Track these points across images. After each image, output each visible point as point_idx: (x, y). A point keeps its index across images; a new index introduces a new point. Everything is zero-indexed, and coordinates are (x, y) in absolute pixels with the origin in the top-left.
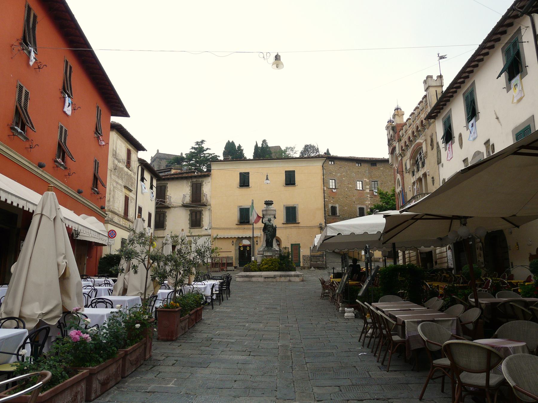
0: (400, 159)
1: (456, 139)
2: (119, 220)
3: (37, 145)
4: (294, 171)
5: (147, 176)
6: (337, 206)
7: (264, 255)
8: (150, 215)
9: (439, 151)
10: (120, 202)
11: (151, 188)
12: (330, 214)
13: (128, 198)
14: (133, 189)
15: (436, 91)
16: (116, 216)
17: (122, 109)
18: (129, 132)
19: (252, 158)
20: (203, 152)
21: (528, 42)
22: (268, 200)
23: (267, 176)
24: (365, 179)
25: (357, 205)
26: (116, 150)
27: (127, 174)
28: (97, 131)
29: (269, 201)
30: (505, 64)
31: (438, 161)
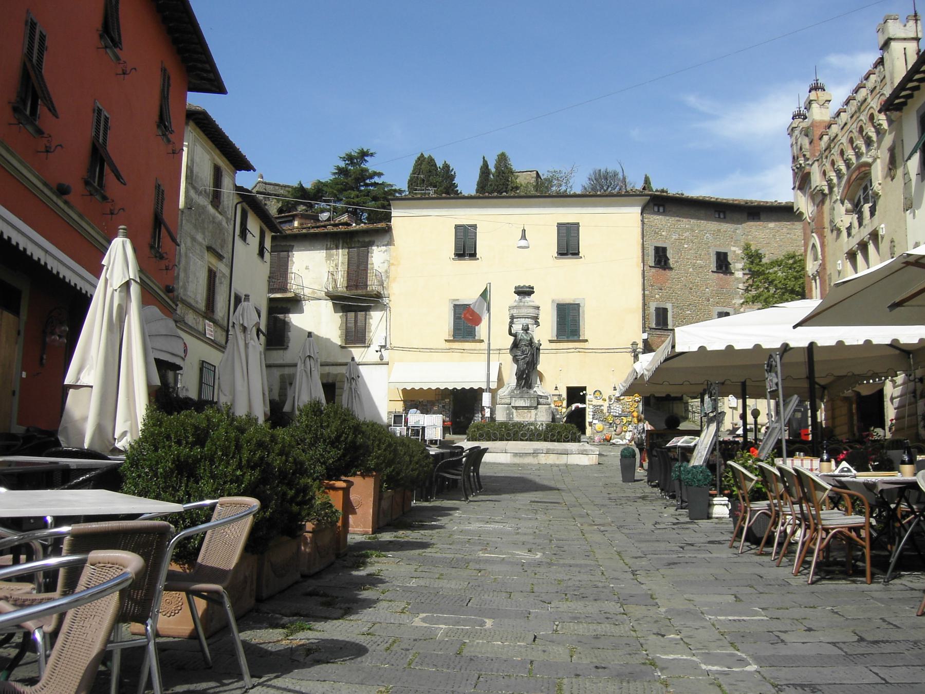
2: (196, 320)
3: (61, 145)
4: (578, 224)
5: (254, 225)
6: (669, 306)
7: (513, 405)
10: (198, 282)
11: (261, 254)
12: (654, 326)
14: (225, 256)
16: (191, 311)
18: (220, 127)
19: (473, 192)
22: (522, 285)
23: (524, 231)
24: (733, 249)
26: (193, 165)
27: (213, 221)
28: (163, 122)
30: (64, 413)
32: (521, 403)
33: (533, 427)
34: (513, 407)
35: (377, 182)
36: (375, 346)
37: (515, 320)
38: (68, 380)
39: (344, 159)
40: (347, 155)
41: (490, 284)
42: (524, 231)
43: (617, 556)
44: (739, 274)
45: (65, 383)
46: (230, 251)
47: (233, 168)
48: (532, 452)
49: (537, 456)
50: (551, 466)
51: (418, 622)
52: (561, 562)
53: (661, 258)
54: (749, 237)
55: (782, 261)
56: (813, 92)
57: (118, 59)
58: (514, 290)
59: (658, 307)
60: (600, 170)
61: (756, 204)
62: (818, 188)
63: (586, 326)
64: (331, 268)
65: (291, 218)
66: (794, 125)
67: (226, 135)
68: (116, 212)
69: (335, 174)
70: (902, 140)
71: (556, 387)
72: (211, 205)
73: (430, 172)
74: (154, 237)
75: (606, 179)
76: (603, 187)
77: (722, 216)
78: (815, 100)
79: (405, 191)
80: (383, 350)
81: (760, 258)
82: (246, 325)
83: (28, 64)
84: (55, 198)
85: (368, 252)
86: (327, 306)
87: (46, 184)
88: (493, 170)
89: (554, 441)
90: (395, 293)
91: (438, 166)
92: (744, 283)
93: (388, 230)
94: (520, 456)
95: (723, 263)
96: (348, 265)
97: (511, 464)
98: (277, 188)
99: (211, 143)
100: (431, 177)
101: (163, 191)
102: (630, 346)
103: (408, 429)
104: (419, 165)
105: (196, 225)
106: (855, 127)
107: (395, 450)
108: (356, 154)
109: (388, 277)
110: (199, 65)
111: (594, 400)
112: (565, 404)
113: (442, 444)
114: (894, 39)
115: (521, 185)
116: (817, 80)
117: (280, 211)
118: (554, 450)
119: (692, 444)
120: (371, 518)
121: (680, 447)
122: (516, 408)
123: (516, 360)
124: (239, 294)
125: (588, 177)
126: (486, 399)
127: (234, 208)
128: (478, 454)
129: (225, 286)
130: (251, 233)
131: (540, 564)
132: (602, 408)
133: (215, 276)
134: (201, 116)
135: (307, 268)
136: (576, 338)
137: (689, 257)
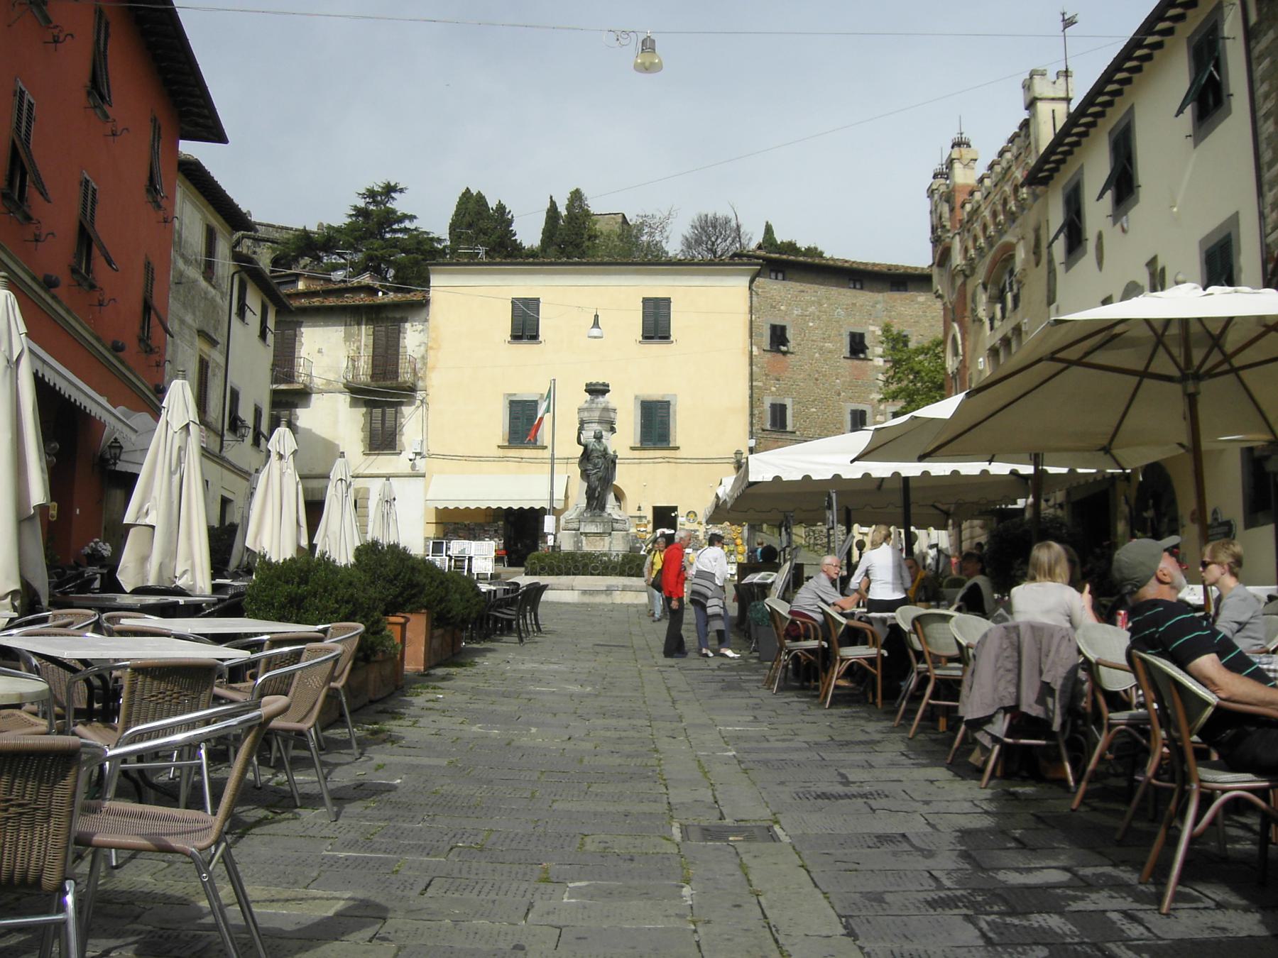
0: (959, 281)
1: (1091, 245)
5: (254, 300)
6: (788, 402)
7: (582, 530)
8: (258, 413)
9: (1052, 272)
11: (263, 335)
12: (768, 427)
13: (207, 363)
14: (219, 340)
15: (1053, 111)
17: (210, 121)
20: (392, 225)
21: (1234, 38)
22: (594, 382)
23: (596, 316)
24: (872, 328)
25: (845, 401)
26: (182, 229)
29: (597, 384)
31: (1049, 297)
32: (591, 528)
33: (606, 558)
34: (582, 534)
35: (408, 227)
36: (408, 454)
37: (585, 425)
38: (128, 518)
39: (363, 196)
40: (368, 190)
41: (554, 380)
42: (596, 316)
43: (666, 691)
44: (879, 362)
45: (125, 522)
46: (226, 330)
47: (230, 229)
48: (605, 589)
49: (611, 594)
50: (628, 605)
51: (475, 728)
52: (608, 694)
53: (778, 337)
54: (893, 313)
55: (929, 349)
56: (956, 149)
57: (107, 117)
58: (585, 388)
59: (774, 402)
60: (706, 216)
61: (902, 271)
62: (959, 268)
63: (678, 430)
64: (351, 352)
65: (293, 278)
66: (934, 187)
67: (206, 171)
68: (106, 302)
69: (351, 216)
70: (1048, 221)
71: (639, 507)
72: (203, 277)
73: (480, 214)
74: (143, 328)
75: (715, 227)
76: (710, 238)
77: (858, 286)
78: (958, 159)
79: (445, 240)
80: (418, 457)
81: (906, 344)
82: (282, 452)
83: (17, 142)
84: (43, 294)
85: (399, 332)
86: (344, 399)
87: (34, 279)
88: (564, 212)
89: (632, 576)
90: (436, 384)
91: (490, 206)
92: (883, 374)
93: (424, 304)
94: (590, 594)
95: (858, 346)
96: (374, 348)
97: (578, 604)
98: (271, 229)
99: (202, 198)
100: (481, 221)
101: (153, 269)
102: (733, 456)
103: (450, 560)
104: (463, 203)
105: (184, 303)
106: (996, 198)
107: (447, 588)
108: (379, 190)
109: (425, 364)
110: (195, 110)
111: (687, 523)
112: (650, 528)
113: (495, 577)
114: (1041, 99)
115: (602, 233)
116: (961, 134)
117: (276, 262)
118: (631, 586)
119: (769, 581)
120: (423, 656)
121: (756, 584)
122: (586, 534)
123: (585, 475)
124: (236, 388)
125: (691, 223)
126: (549, 523)
127: (230, 279)
128: (538, 590)
129: (219, 378)
130: (251, 310)
131: (589, 695)
132: (697, 533)
133: (207, 367)
134: (193, 167)
135: (320, 351)
136: (664, 445)
137: (814, 338)
